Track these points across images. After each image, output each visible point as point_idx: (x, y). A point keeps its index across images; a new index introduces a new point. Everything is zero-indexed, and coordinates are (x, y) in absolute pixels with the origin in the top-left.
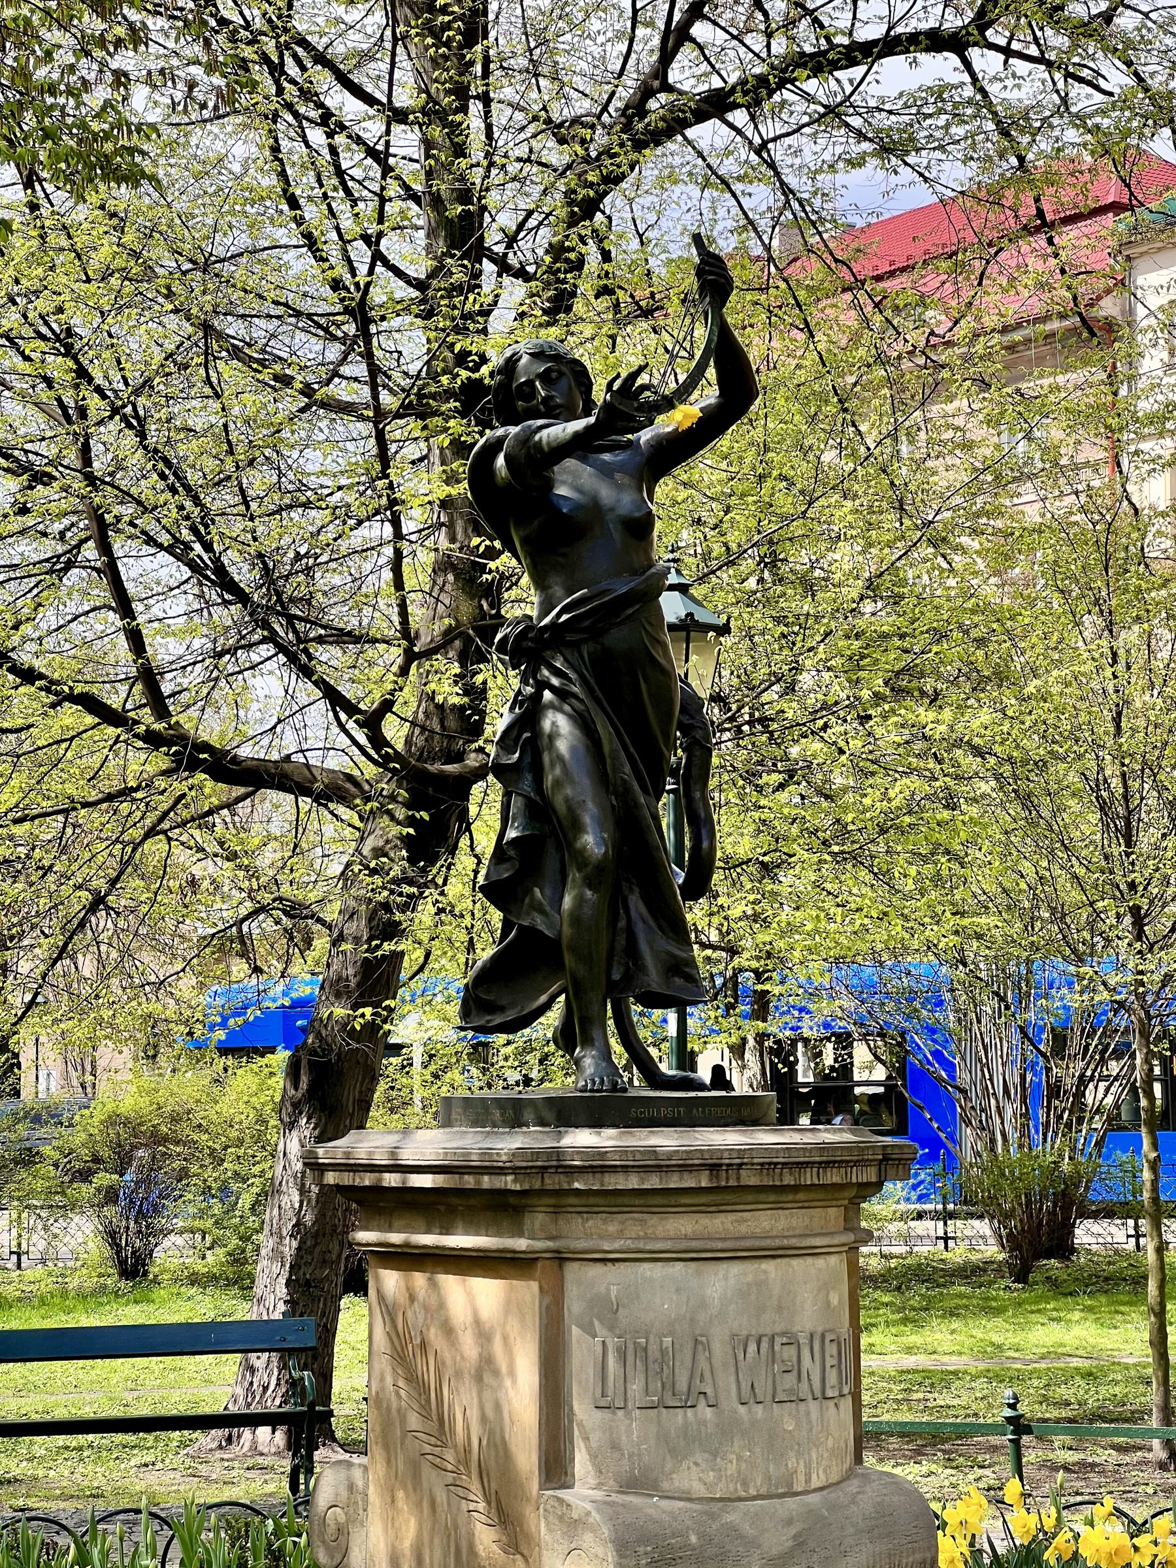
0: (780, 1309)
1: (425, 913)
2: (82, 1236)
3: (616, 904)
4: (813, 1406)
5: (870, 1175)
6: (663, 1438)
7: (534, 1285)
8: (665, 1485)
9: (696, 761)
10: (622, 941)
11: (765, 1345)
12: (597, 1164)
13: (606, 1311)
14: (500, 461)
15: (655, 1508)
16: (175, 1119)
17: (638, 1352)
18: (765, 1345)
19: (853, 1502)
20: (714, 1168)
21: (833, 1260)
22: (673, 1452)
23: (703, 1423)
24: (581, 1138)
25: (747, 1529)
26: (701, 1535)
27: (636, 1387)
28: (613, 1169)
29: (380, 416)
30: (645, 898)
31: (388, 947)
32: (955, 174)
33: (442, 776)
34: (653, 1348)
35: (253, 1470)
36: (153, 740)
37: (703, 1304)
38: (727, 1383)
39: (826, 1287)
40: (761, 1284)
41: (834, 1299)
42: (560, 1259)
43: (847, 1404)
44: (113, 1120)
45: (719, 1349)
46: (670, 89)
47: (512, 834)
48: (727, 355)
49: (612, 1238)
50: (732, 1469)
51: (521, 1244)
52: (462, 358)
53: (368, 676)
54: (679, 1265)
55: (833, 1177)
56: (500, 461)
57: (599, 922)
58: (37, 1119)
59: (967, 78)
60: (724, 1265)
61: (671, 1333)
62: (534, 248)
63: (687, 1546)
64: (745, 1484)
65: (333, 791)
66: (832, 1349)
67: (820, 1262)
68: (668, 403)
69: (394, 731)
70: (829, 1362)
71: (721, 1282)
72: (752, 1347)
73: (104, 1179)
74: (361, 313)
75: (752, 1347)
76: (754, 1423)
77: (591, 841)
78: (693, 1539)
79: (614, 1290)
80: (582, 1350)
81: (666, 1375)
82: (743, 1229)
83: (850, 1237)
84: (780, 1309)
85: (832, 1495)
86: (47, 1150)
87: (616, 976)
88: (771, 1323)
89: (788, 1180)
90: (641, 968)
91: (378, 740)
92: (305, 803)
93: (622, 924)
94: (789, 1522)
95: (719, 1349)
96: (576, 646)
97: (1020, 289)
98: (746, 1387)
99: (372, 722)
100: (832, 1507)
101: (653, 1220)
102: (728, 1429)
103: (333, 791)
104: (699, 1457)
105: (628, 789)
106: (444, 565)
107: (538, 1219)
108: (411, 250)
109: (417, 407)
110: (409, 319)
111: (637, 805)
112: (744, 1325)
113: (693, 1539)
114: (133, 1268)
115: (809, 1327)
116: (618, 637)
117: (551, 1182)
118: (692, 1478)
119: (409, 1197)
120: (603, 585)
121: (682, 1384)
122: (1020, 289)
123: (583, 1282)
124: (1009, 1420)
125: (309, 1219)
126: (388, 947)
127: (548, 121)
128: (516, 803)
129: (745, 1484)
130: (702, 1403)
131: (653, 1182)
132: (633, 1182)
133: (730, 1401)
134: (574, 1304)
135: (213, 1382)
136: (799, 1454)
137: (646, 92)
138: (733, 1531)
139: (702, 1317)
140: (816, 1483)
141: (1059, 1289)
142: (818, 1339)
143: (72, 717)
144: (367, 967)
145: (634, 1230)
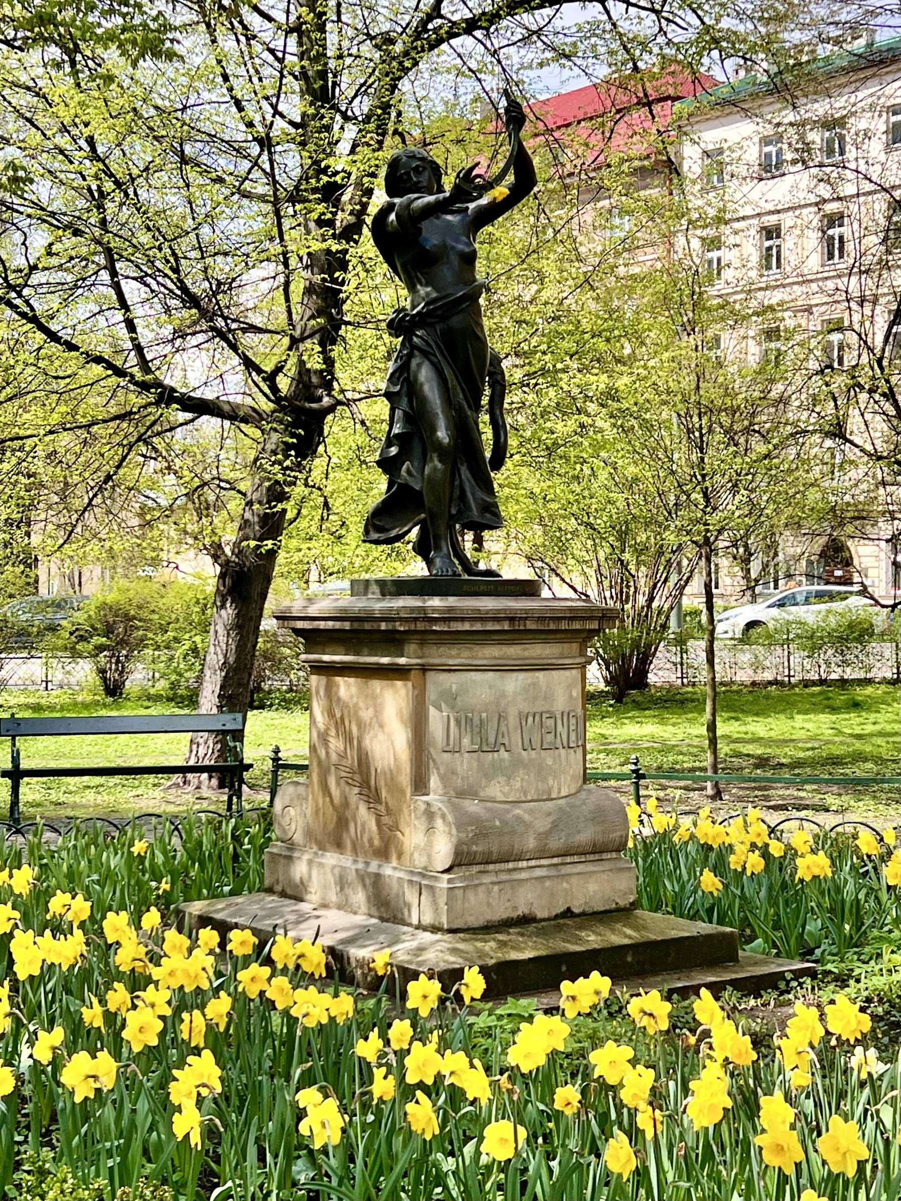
0: (546, 698)
1: (299, 490)
2: (84, 672)
3: (453, 472)
4: (563, 752)
5: (594, 625)
6: (481, 766)
7: (410, 684)
8: (482, 794)
9: (497, 392)
10: (457, 492)
11: (537, 718)
12: (449, 616)
13: (450, 699)
14: (392, 217)
15: (472, 806)
16: (140, 607)
17: (467, 721)
18: (537, 718)
19: (584, 803)
20: (512, 619)
21: (574, 672)
22: (486, 775)
23: (502, 760)
24: (436, 602)
25: (526, 817)
26: (501, 821)
27: (466, 741)
28: (463, 619)
29: (276, 202)
30: (470, 469)
31: (280, 507)
32: (602, 71)
33: (311, 409)
34: (476, 721)
35: (208, 794)
36: (144, 386)
37: (503, 695)
38: (516, 738)
39: (570, 687)
40: (535, 685)
41: (574, 694)
42: (424, 669)
43: (580, 751)
44: (103, 606)
45: (512, 720)
46: (442, 17)
47: (396, 430)
48: (521, 163)
49: (452, 657)
50: (518, 785)
51: (402, 661)
52: (324, 171)
53: (268, 351)
54: (491, 674)
55: (577, 625)
56: (392, 217)
57: (440, 486)
58: (59, 606)
59: (605, 17)
60: (515, 674)
61: (486, 711)
62: (362, 106)
63: (494, 827)
64: (525, 794)
65: (253, 417)
66: (573, 721)
67: (567, 673)
68: (489, 186)
69: (283, 383)
70: (572, 728)
71: (514, 683)
72: (530, 719)
73: (98, 640)
74: (266, 143)
75: (530, 719)
76: (531, 760)
77: (442, 434)
78: (498, 823)
79: (454, 687)
80: (436, 719)
81: (483, 732)
82: (526, 654)
83: (582, 660)
84: (546, 698)
85: (571, 800)
86: (64, 623)
87: (454, 512)
88: (540, 706)
89: (552, 627)
90: (469, 508)
91: (274, 389)
92: (227, 423)
93: (457, 483)
94: (549, 814)
95: (512, 720)
96: (432, 325)
97: (632, 142)
98: (526, 742)
99: (271, 379)
100: (572, 806)
101: (477, 648)
102: (517, 763)
103: (253, 417)
104: (501, 779)
105: (461, 408)
106: (309, 290)
107: (411, 648)
108: (294, 106)
109: (294, 198)
110: (293, 146)
111: (466, 417)
112: (525, 707)
113: (498, 823)
114: (114, 690)
115: (561, 708)
116: (457, 321)
117: (421, 626)
118: (496, 790)
119: (335, 635)
120: (449, 291)
121: (492, 739)
122: (632, 142)
123: (438, 682)
124: (633, 771)
125: (231, 660)
126: (280, 507)
127: (368, 34)
128: (398, 413)
129: (525, 794)
130: (502, 749)
131: (478, 627)
132: (467, 626)
133: (517, 748)
134: (432, 693)
135: (174, 749)
136: (555, 777)
137: (430, 18)
138: (518, 818)
139: (503, 702)
140: (563, 794)
141: (639, 706)
142: (567, 715)
143: (98, 370)
144: (265, 519)
145: (466, 653)
